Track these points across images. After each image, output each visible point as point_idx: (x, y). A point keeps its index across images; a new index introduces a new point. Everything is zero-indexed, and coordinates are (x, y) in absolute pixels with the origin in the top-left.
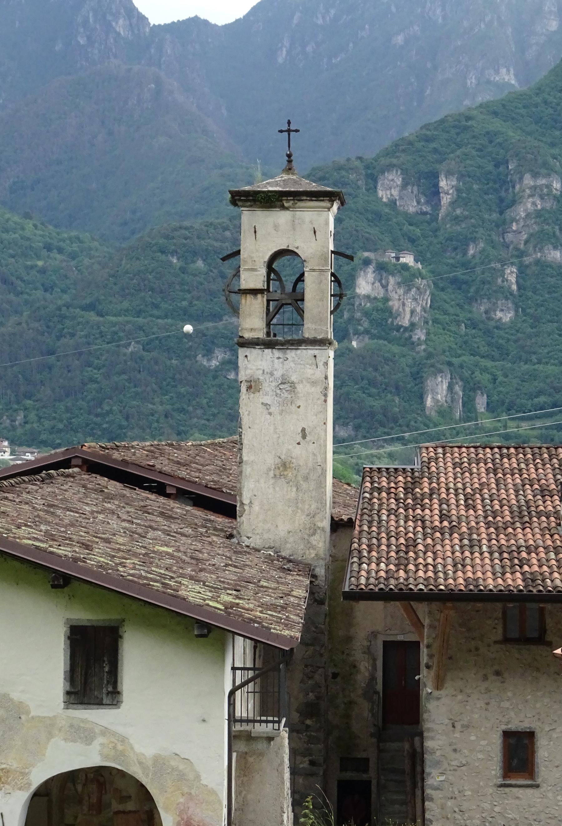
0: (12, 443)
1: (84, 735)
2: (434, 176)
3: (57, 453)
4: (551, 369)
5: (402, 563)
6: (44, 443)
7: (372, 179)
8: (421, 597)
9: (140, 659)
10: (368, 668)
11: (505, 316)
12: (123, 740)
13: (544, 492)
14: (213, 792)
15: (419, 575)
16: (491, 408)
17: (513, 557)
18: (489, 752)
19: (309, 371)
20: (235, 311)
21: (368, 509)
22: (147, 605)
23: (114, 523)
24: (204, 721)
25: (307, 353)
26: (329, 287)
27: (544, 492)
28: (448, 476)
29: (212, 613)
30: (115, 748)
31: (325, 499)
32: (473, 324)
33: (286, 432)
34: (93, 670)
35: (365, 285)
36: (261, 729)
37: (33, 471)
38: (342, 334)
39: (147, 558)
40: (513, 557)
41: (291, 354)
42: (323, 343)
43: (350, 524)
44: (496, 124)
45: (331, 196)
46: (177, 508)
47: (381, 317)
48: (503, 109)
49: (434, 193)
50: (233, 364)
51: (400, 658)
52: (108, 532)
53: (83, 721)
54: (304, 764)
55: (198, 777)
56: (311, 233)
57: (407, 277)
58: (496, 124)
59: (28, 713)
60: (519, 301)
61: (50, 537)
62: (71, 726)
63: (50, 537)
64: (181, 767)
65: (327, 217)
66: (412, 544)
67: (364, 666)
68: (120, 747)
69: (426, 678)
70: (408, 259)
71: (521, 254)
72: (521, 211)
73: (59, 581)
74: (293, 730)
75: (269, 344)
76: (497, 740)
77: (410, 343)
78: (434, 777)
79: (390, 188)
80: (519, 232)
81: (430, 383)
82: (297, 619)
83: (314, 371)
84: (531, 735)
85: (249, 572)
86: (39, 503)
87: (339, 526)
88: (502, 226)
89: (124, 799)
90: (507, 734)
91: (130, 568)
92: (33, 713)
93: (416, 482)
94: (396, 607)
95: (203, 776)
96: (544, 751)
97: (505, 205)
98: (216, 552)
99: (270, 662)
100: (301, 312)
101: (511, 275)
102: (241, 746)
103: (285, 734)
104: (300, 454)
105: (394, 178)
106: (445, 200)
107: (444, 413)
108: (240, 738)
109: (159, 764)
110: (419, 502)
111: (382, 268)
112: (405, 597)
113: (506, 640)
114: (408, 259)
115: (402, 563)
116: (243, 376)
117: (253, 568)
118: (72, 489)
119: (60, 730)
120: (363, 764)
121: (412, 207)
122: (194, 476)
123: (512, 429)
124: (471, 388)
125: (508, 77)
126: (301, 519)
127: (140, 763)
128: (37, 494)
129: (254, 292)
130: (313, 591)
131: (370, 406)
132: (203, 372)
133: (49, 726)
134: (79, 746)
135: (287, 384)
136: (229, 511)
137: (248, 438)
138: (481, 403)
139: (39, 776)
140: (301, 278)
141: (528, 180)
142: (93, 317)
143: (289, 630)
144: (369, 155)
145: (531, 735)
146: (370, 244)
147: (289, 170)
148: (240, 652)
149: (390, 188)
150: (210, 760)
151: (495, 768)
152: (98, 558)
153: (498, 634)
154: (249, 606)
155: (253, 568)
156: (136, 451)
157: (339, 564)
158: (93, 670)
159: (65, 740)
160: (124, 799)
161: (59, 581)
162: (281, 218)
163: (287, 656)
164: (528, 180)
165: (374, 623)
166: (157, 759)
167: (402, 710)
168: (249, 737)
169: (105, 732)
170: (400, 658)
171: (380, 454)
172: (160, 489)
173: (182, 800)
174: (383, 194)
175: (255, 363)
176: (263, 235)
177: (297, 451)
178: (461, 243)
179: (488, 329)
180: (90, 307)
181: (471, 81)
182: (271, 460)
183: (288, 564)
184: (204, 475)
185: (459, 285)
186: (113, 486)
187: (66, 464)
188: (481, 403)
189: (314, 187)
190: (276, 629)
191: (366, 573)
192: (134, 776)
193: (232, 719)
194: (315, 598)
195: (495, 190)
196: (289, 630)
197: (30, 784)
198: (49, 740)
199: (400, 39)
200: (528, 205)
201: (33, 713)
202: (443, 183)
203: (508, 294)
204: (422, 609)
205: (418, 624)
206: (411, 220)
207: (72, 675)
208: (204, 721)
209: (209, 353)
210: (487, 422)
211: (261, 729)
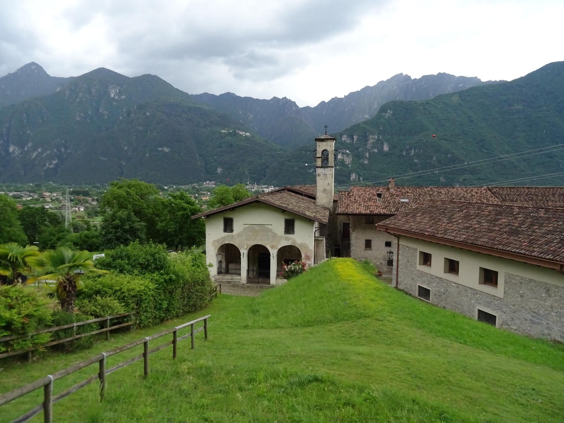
0: (274, 186)
1: (288, 239)
2: (353, 136)
3: (283, 188)
4: (375, 172)
5: (347, 208)
6: (279, 186)
7: (341, 136)
8: (350, 214)
9: (298, 226)
10: (340, 228)
11: (366, 162)
12: (295, 240)
13: (374, 195)
15: (350, 211)
16: (363, 179)
17: (368, 207)
18: (362, 243)
19: (329, 172)
20: (316, 161)
21: (340, 198)
22: (32, 389)
23: (293, 201)
25: (329, 169)
26: (333, 157)
27: (374, 195)
28: (355, 192)
29: (311, 217)
31: (332, 196)
32: (360, 164)
33: (325, 183)
34: (289, 228)
35: (339, 157)
36: (320, 239)
37: (278, 191)
38: (335, 166)
39: (299, 207)
40: (368, 207)
41: (326, 169)
42: (332, 167)
43: (337, 201)
44: (365, 126)
45: (334, 139)
46: (305, 198)
47: (342, 162)
48: (366, 122)
49: (353, 139)
50: (315, 171)
51: (346, 226)
52: (293, 202)
54: (328, 245)
56: (330, 146)
57: (347, 155)
58: (365, 126)
60: (369, 159)
61: (281, 203)
63: (281, 203)
65: (333, 143)
66: (349, 205)
67: (339, 227)
69: (351, 229)
70: (348, 152)
71: (369, 150)
72: (369, 142)
73: (283, 211)
74: (326, 239)
75: (322, 167)
76: (364, 242)
77: (348, 168)
78: (352, 248)
79: (344, 138)
80: (369, 146)
81: (352, 175)
82: (327, 218)
83: (331, 172)
84: (370, 241)
85: (318, 210)
86: (279, 197)
87: (335, 201)
88: (366, 145)
89: (295, 251)
90: (366, 240)
91: (296, 209)
93: (349, 193)
94: (345, 216)
96: (373, 244)
97: (366, 141)
98: (312, 206)
99: (322, 226)
100: (328, 161)
101: (367, 154)
102: (317, 242)
103: (325, 240)
104: (328, 188)
105: (345, 136)
106: (355, 140)
107: (354, 181)
108: (316, 240)
109: (301, 245)
110: (350, 197)
111: (343, 153)
112: (347, 214)
113: (366, 223)
114: (348, 152)
115: (347, 208)
116: (317, 173)
117: (319, 209)
118: (285, 194)
120: (339, 245)
121: (349, 142)
122: (308, 192)
123: (367, 183)
124: (360, 176)
125: (367, 116)
126: (328, 200)
128: (279, 195)
129: (319, 158)
130: (330, 213)
131: (341, 179)
132: (309, 173)
133: (281, 237)
134: (286, 241)
135: (325, 175)
136: (314, 198)
137: (318, 185)
138: (361, 179)
139: (280, 246)
140: (328, 155)
141: (371, 136)
142: (288, 163)
143: (326, 220)
144: (341, 132)
145: (370, 241)
146: (340, 149)
147: (326, 134)
148: (316, 224)
149: (344, 138)
150: (311, 244)
151: (364, 246)
152: (290, 207)
153: (365, 221)
154: (318, 216)
155: (319, 209)
156: (297, 187)
157: (335, 208)
158: (289, 228)
160: (295, 251)
161: (283, 211)
162: (324, 143)
163: (325, 225)
164: (371, 136)
165: (341, 219)
166: (301, 244)
167: (346, 236)
168: (318, 240)
169: (292, 239)
170: (346, 226)
171: (342, 188)
172: (301, 194)
174: (343, 139)
175: (319, 171)
176: (321, 147)
177: (327, 187)
178: (358, 148)
179: (363, 165)
180: (288, 161)
181: (360, 117)
182: (322, 189)
183: (326, 208)
184: (310, 192)
185: (357, 156)
186: (293, 194)
187: (284, 190)
188: (361, 179)
189: (331, 138)
190: (323, 220)
191: (340, 210)
192: (45, 69)
193: (315, 237)
194: (330, 215)
195: (365, 138)
196: (326, 220)
199: (346, 110)
200: (371, 141)
202: (354, 137)
203: (366, 158)
204: (350, 217)
205: (349, 220)
206: (348, 144)
207: (285, 228)
209: (310, 170)
210: (362, 182)
211: (320, 239)
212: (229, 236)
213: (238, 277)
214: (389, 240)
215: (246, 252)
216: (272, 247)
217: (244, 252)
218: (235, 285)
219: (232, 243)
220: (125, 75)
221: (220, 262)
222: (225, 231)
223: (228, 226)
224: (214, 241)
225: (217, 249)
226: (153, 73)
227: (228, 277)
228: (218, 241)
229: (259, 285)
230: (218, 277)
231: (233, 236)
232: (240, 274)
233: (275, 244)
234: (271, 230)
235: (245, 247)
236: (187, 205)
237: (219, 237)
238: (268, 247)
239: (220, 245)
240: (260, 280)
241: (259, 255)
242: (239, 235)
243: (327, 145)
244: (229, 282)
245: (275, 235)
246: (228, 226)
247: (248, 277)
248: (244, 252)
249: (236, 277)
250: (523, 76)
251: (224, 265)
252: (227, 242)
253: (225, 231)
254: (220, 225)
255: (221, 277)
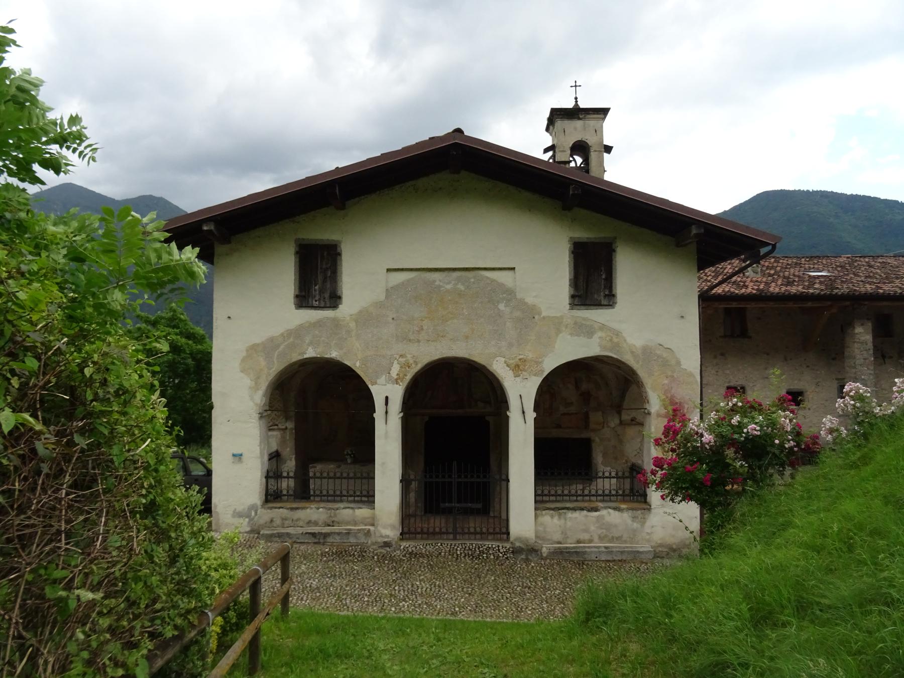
1: (586, 330)
9: (632, 270)
12: (618, 334)
14: (691, 375)
24: (682, 317)
30: (611, 340)
34: (592, 280)
53: (584, 319)
55: (678, 363)
59: (539, 313)
62: (575, 323)
64: (665, 355)
68: (615, 340)
92: (544, 314)
95: (683, 361)
102: (371, 493)
109: (647, 352)
113: (725, 336)
119: (566, 327)
127: (632, 352)
133: (557, 324)
139: (550, 364)
158: (592, 280)
159: (571, 334)
162: (578, 124)
169: (603, 327)
173: (666, 382)
197: (543, 371)
198: (557, 335)
201: (544, 314)
207: (575, 282)
208: (682, 317)
212: (319, 324)
213: (363, 512)
214: (796, 386)
215: (397, 394)
216: (517, 369)
217: (388, 394)
218: (348, 552)
219: (334, 354)
220: (109, 196)
221: (275, 457)
222: (303, 300)
223: (318, 278)
224: (253, 348)
225: (264, 384)
226: (157, 194)
227: (313, 514)
228: (268, 347)
229: (459, 545)
230: (265, 515)
231: (336, 324)
232: (368, 498)
233: (530, 356)
234: (510, 294)
235: (395, 370)
236: (184, 340)
237: (276, 330)
238: (500, 369)
239: (277, 366)
240: (437, 522)
241: (454, 414)
242: (365, 318)
243: (584, 128)
244: (318, 538)
245: (529, 314)
246: (318, 278)
247: (406, 516)
248: (388, 394)
249: (351, 514)
250: (727, 209)
251: (290, 465)
252: (310, 353)
253: (303, 300)
254: (280, 273)
255: (279, 513)
